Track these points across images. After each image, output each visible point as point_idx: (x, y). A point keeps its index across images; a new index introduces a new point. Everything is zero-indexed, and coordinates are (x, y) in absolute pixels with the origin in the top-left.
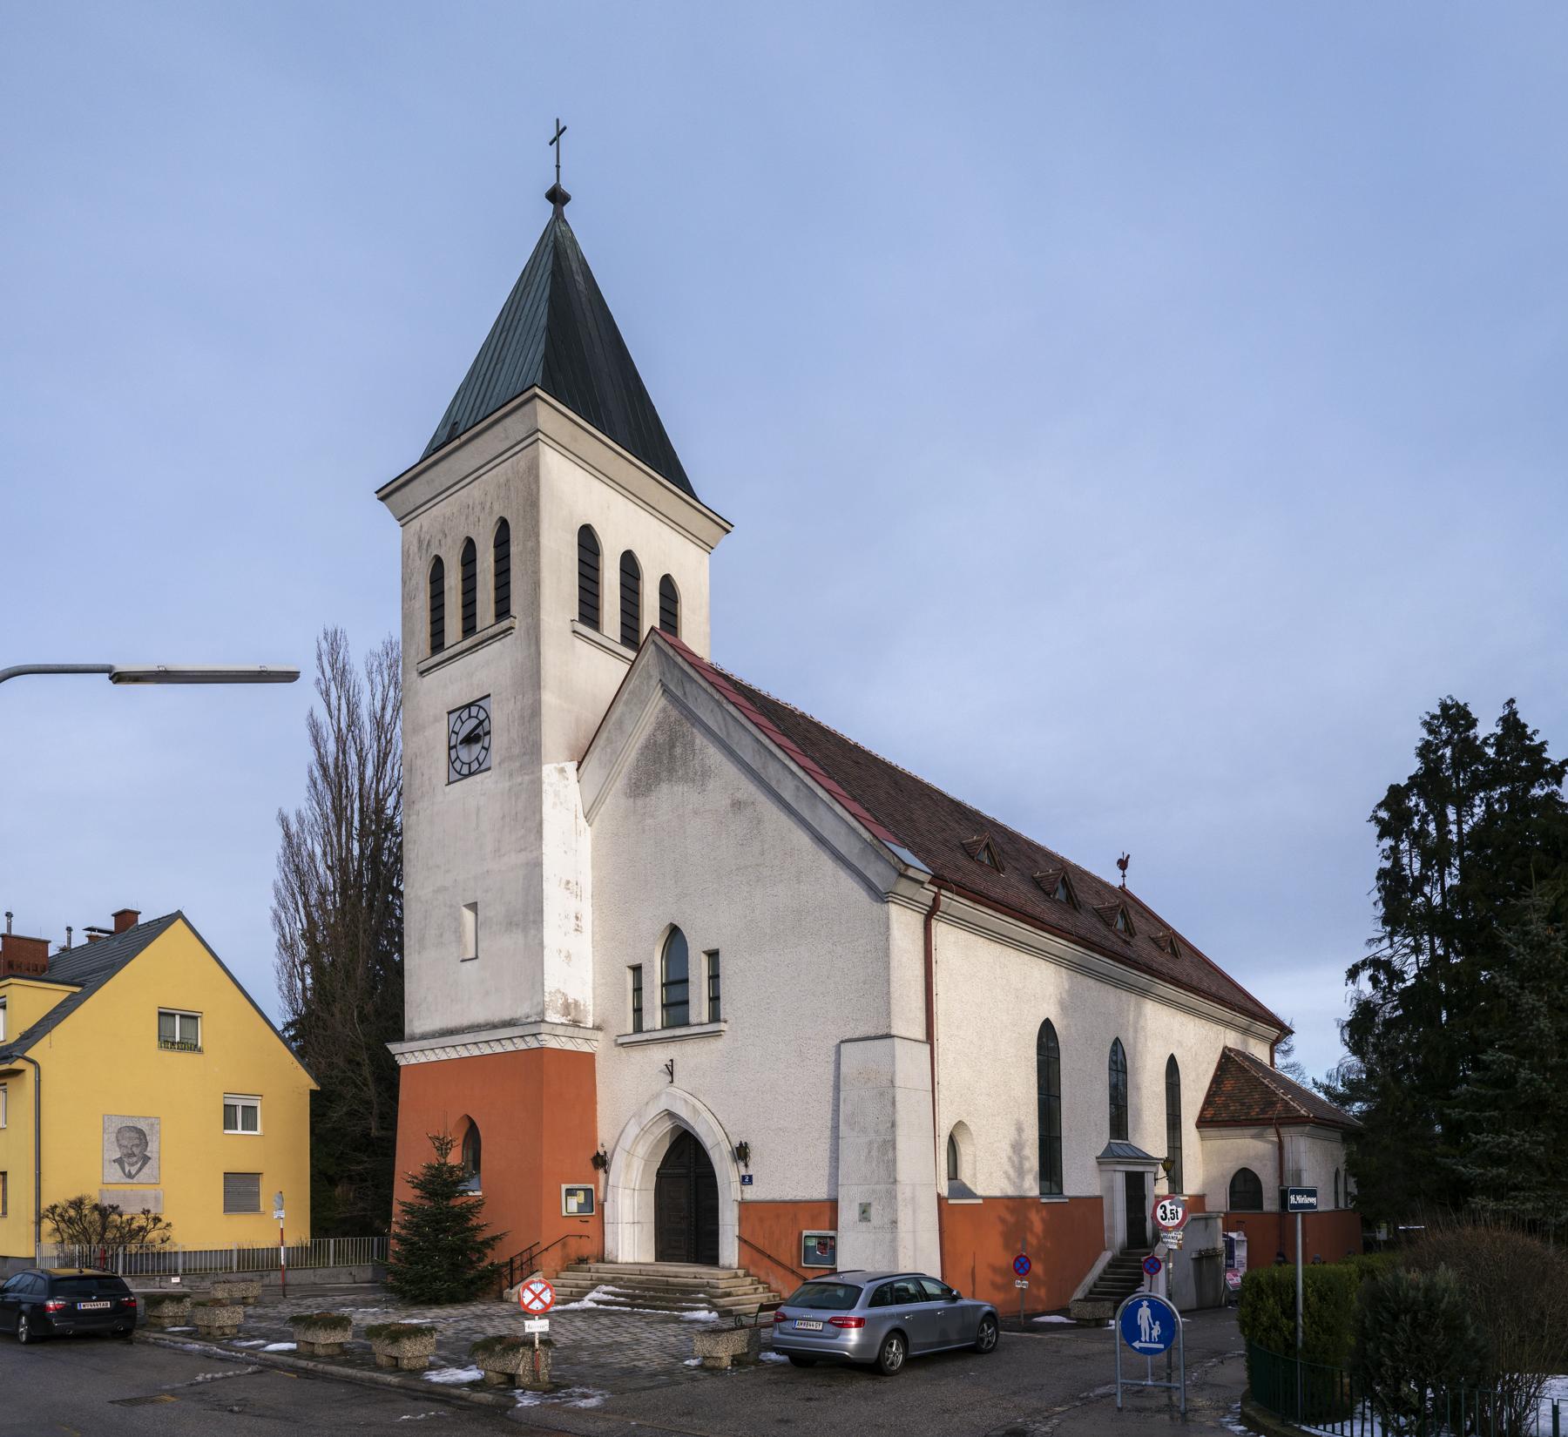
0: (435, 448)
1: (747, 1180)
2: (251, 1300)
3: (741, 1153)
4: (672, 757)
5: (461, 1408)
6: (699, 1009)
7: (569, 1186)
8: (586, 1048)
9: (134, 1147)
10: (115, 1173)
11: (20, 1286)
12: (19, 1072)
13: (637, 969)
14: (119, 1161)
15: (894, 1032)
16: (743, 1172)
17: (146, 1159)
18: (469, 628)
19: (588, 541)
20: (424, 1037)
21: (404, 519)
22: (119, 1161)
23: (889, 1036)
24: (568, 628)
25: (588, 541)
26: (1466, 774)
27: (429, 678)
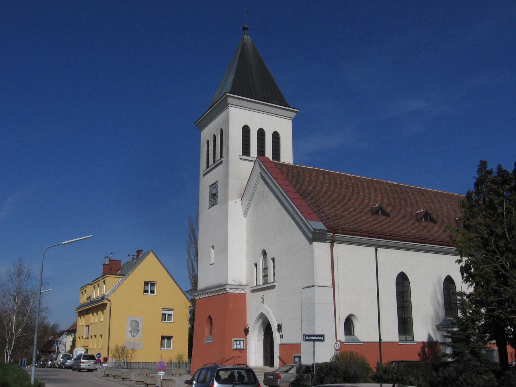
1: (282, 337)
2: (224, 375)
3: (280, 327)
7: (235, 339)
8: (243, 292)
9: (135, 328)
10: (129, 336)
12: (106, 304)
13: (256, 265)
14: (131, 331)
15: (315, 284)
17: (138, 331)
19: (246, 130)
22: (131, 331)
23: (313, 286)
24: (239, 157)
25: (246, 130)
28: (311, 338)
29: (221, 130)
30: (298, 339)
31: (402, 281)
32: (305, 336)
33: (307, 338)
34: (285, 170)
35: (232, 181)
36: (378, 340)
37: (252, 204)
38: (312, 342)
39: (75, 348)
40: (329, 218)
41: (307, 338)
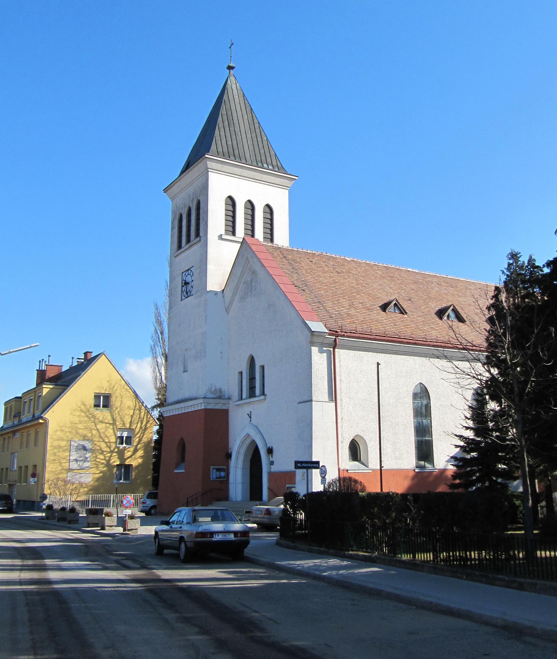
0: (183, 172)
3: (270, 451)
4: (252, 287)
5: (32, 506)
6: (258, 391)
7: (214, 467)
11: (197, 630)
16: (271, 460)
18: (188, 241)
19: (231, 202)
20: (172, 404)
21: (172, 199)
25: (231, 202)
26: (521, 277)
27: (178, 258)
28: (304, 465)
29: (199, 203)
30: (291, 467)
31: (422, 395)
32: (296, 463)
33: (299, 465)
34: (278, 255)
35: (211, 267)
36: (378, 467)
37: (236, 297)
38: (305, 470)
39: (154, 464)
40: (331, 317)
41: (299, 465)
